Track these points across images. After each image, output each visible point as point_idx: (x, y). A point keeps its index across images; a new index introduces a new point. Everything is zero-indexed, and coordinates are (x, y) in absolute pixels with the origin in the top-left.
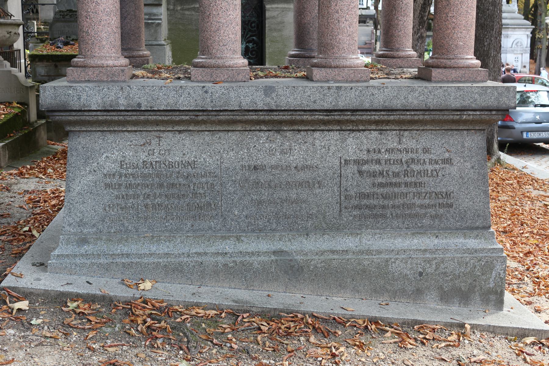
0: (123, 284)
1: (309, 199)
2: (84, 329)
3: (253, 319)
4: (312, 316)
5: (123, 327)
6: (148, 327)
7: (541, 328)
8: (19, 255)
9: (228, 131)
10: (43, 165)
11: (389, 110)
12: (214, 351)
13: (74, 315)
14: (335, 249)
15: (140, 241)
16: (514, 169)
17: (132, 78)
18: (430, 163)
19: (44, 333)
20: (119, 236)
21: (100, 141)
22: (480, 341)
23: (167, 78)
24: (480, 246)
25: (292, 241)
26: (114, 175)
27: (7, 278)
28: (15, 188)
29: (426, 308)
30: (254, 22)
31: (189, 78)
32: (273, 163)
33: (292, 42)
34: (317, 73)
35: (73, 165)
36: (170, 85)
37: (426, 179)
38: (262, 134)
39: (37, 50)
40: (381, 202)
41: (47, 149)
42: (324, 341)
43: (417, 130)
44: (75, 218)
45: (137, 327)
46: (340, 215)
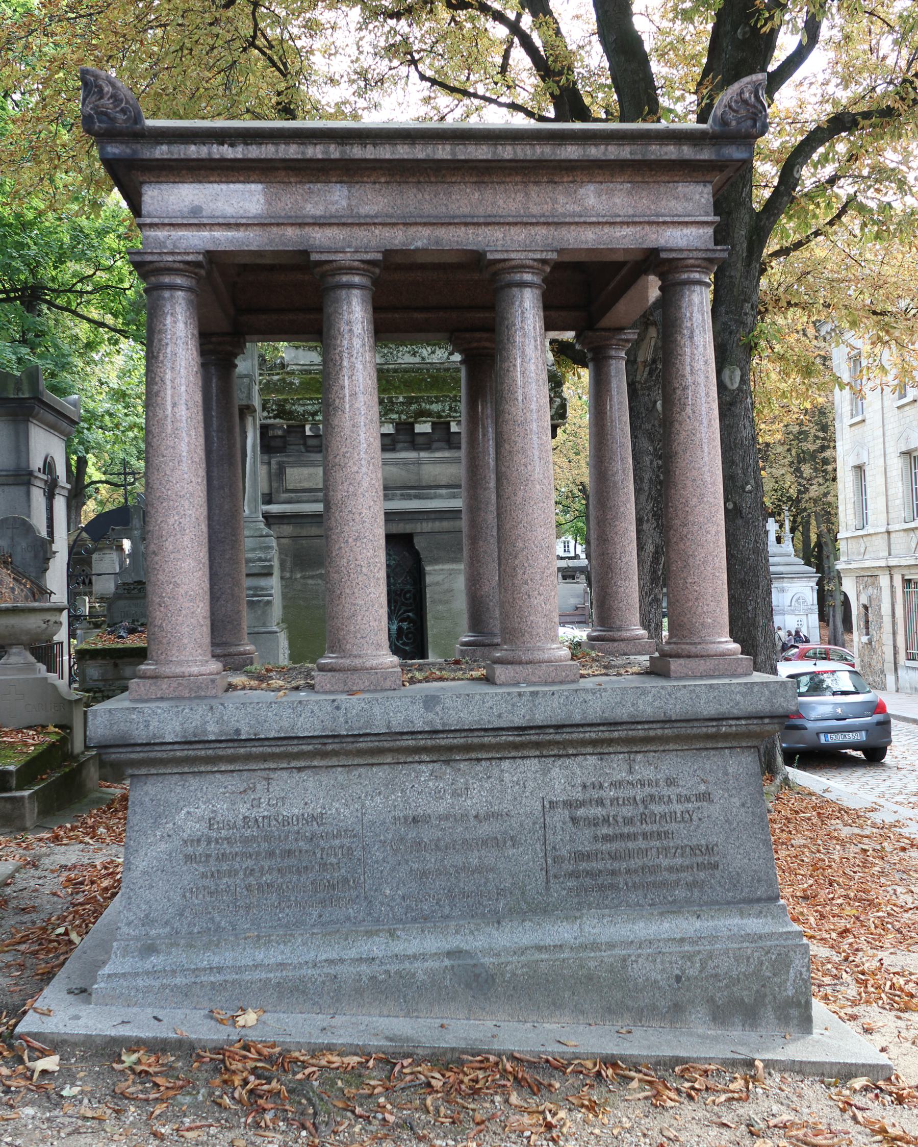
0: (212, 1018)
1: (499, 865)
2: (147, 1100)
3: (419, 1069)
4: (512, 1058)
5: (211, 1094)
6: (251, 1091)
7: (875, 1062)
8: (47, 977)
9: (373, 765)
10: (90, 821)
11: (610, 724)
12: (357, 1129)
13: (132, 1077)
14: (542, 943)
15: (239, 945)
16: (810, 794)
17: (227, 691)
18: (679, 801)
19: (82, 1112)
20: (205, 939)
21: (179, 789)
22: (780, 1089)
23: (279, 689)
24: (767, 930)
25: (476, 933)
26: (199, 841)
27: (26, 1018)
28: (46, 862)
29: (691, 1035)
30: (409, 591)
31: (312, 687)
32: (441, 810)
33: (464, 621)
34: (501, 672)
35: (136, 828)
36: (284, 699)
37: (673, 826)
38: (423, 767)
39: (88, 643)
40: (608, 866)
41: (99, 795)
42: (533, 1101)
43: (655, 752)
44: (138, 911)
45: (232, 1093)
46: (547, 889)
